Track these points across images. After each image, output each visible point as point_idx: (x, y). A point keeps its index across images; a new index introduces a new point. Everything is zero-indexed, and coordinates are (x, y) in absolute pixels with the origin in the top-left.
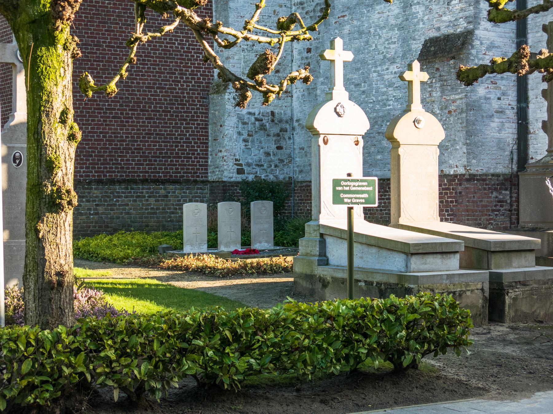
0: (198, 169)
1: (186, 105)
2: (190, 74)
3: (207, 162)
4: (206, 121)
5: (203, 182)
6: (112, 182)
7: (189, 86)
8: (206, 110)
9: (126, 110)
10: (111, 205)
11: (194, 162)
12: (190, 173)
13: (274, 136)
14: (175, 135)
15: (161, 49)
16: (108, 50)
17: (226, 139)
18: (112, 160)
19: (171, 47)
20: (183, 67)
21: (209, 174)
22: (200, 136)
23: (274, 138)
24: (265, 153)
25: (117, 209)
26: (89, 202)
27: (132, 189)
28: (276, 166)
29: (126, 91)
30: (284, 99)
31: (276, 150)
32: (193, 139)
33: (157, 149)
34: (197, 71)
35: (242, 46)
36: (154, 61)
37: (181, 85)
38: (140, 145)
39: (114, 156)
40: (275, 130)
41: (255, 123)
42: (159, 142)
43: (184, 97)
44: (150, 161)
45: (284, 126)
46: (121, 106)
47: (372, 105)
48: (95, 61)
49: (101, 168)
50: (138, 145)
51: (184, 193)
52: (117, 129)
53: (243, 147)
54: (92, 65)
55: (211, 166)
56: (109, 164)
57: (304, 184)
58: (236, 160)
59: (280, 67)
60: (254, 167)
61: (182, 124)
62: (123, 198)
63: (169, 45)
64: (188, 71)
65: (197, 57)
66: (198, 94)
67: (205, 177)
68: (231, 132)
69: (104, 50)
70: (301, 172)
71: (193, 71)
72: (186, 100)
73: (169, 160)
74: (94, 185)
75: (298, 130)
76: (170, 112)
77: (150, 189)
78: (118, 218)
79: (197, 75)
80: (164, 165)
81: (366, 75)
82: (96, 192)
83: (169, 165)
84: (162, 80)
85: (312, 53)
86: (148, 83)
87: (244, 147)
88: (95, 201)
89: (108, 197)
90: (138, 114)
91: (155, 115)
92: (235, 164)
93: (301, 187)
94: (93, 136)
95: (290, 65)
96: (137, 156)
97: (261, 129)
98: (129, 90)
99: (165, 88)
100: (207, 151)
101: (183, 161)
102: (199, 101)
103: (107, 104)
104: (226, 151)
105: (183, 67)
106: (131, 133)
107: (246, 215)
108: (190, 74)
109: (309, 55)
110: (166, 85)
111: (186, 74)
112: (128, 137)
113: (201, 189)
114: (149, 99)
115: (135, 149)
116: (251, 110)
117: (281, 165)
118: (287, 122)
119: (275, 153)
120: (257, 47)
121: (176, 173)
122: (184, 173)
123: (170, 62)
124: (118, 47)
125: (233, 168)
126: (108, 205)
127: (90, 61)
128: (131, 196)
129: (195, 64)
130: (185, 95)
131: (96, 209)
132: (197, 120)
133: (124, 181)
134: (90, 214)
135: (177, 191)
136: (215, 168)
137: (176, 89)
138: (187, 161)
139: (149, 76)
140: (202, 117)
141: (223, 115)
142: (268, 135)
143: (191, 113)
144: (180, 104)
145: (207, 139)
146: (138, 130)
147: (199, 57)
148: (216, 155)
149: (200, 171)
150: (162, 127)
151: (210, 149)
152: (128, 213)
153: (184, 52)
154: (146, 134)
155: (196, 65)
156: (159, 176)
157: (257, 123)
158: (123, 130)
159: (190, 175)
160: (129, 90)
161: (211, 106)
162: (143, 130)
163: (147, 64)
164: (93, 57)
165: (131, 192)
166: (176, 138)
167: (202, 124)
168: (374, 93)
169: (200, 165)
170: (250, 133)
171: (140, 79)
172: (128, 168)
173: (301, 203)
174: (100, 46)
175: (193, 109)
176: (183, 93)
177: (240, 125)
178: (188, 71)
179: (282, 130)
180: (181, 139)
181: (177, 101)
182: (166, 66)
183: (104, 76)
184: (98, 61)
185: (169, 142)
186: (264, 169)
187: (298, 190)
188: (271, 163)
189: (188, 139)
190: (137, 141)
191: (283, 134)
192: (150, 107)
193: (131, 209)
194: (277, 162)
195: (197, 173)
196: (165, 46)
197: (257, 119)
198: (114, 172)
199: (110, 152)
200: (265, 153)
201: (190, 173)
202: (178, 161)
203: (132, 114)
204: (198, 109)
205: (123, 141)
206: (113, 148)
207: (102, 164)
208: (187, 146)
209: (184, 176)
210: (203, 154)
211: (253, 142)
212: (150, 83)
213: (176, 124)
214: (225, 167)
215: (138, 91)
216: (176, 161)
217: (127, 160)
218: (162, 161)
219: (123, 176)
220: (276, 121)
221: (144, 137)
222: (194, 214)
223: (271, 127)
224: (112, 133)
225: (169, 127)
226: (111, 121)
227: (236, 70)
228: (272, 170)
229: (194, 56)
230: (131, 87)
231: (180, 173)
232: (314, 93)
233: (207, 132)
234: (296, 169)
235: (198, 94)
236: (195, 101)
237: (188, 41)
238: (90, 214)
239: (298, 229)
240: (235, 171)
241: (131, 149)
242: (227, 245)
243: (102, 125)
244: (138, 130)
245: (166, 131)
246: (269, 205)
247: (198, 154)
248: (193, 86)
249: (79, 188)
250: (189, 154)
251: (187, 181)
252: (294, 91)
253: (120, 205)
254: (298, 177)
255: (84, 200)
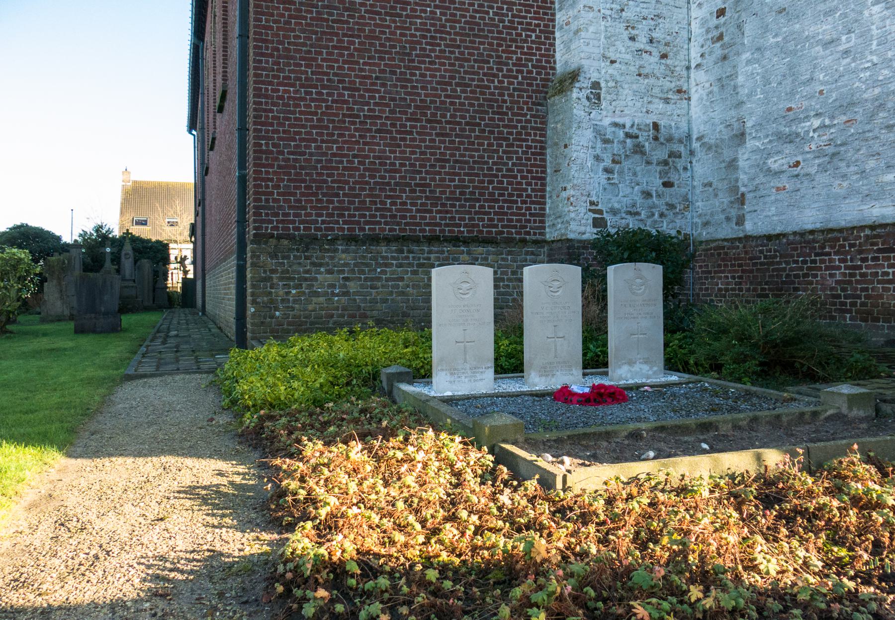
0: (529, 221)
1: (507, 114)
2: (514, 64)
3: (544, 209)
4: (542, 142)
5: (536, 242)
6: (374, 239)
7: (513, 83)
8: (541, 123)
9: (400, 119)
10: (372, 279)
11: (521, 209)
12: (515, 227)
13: (658, 164)
14: (487, 163)
15: (463, 20)
16: (370, 18)
17: (574, 167)
18: (375, 203)
19: (483, 19)
20: (503, 51)
21: (547, 230)
22: (532, 166)
23: (659, 168)
24: (643, 192)
25: (383, 286)
26: (332, 273)
27: (410, 252)
28: (662, 215)
29: (402, 87)
30: (675, 103)
31: (661, 188)
32: (518, 171)
33: (456, 187)
34: (526, 60)
35: (602, 11)
36: (451, 40)
37: (499, 82)
38: (425, 179)
39: (379, 196)
40: (661, 154)
41: (625, 142)
42: (459, 174)
43: (505, 101)
44: (444, 205)
45: (676, 147)
46: (392, 112)
47: (868, 74)
48: (345, 35)
49: (354, 216)
50: (421, 179)
51: (503, 259)
52: (385, 151)
53: (604, 182)
54: (339, 41)
55: (550, 216)
56: (370, 209)
57: (713, 245)
58: (592, 203)
59: (668, 49)
60: (624, 215)
61: (501, 146)
62: (394, 268)
63: (478, 15)
64: (511, 58)
65: (527, 36)
66: (528, 97)
67: (540, 234)
68: (582, 155)
69: (363, 17)
70: (706, 224)
71: (520, 59)
72: (507, 107)
73: (477, 204)
74: (341, 245)
75: (700, 154)
76: (479, 125)
77: (443, 252)
78: (385, 301)
79: (526, 66)
80: (470, 213)
81: (852, 15)
82: (344, 256)
83: (476, 213)
84: (466, 72)
85: (728, 14)
86: (441, 76)
87: (606, 182)
88: (343, 272)
89: (367, 265)
90: (422, 127)
91: (454, 129)
92: (590, 210)
93: (707, 250)
94: (342, 162)
95: (686, 47)
96: (420, 198)
97: (635, 152)
98: (406, 87)
99: (470, 86)
100: (544, 191)
101: (503, 207)
102: (529, 109)
103: (366, 108)
104: (574, 187)
105: (503, 51)
106: (409, 159)
107: (595, 295)
108: (514, 64)
109: (722, 20)
110: (473, 80)
111: (507, 64)
112: (405, 165)
113: (532, 253)
114: (443, 102)
115: (417, 185)
116: (617, 120)
117: (670, 214)
118: (680, 141)
119: (660, 193)
120: (629, 14)
121: (488, 226)
122: (503, 227)
123: (480, 43)
124: (387, 14)
125: (586, 217)
126: (366, 279)
127: (337, 35)
128: (409, 264)
129: (523, 48)
130: (506, 97)
131: (345, 286)
132: (527, 140)
133: (397, 239)
134: (333, 294)
135: (490, 257)
136: (556, 218)
137: (489, 88)
138: (509, 208)
139: (444, 64)
140: (535, 135)
141: (570, 127)
142: (648, 163)
143: (516, 127)
144: (498, 113)
145: (544, 172)
146: (422, 153)
147: (531, 36)
148: (558, 196)
149: (532, 224)
150: (466, 149)
151: (548, 189)
152: (403, 293)
153: (504, 27)
154: (437, 160)
155: (525, 50)
156: (459, 231)
157: (628, 141)
158: (395, 152)
159: (513, 231)
160: (406, 87)
161: (550, 116)
162: (432, 154)
163: (439, 45)
164: (343, 29)
165: (407, 258)
166: (490, 169)
167: (536, 147)
168: (874, 47)
169: (530, 214)
170: (616, 158)
171: (427, 69)
172: (405, 217)
173: (706, 278)
174: (355, 10)
175: (520, 121)
176: (502, 95)
177: (599, 145)
178: (511, 58)
179: (672, 155)
180: (497, 170)
181: (492, 107)
182: (474, 48)
183: (361, 61)
184: (350, 36)
185: (477, 175)
186: (641, 220)
187: (700, 255)
188: (654, 210)
189: (511, 170)
190: (421, 172)
191: (674, 162)
192: (444, 116)
193: (408, 286)
194: (664, 208)
195: (526, 227)
196: (471, 17)
197: (628, 135)
198: (379, 223)
199: (370, 189)
200: (643, 192)
201: (515, 227)
202: (493, 207)
203: (412, 127)
204: (527, 121)
205: (396, 171)
206: (376, 183)
207: (356, 209)
208: (509, 183)
209: (503, 232)
210: (536, 196)
211: (621, 173)
212: (444, 77)
213: (490, 145)
214: (573, 215)
215: (423, 88)
216: (490, 207)
217: (401, 204)
218: (464, 206)
219: (395, 230)
220: (662, 140)
221: (432, 166)
222: (460, 294)
223: (653, 149)
224: (374, 157)
225: (477, 150)
226: (374, 137)
227: (591, 51)
228: (655, 222)
229: (521, 35)
230: (411, 81)
231: (496, 226)
232: (732, 83)
233: (544, 160)
234: (696, 220)
235: (528, 97)
236: (522, 109)
237: (512, 10)
238: (333, 294)
239: (725, 331)
240: (590, 221)
241: (409, 185)
242: (546, 371)
243: (358, 143)
244: (422, 153)
245: (472, 157)
246: (651, 275)
247: (528, 196)
248: (519, 83)
249: (314, 249)
250: (513, 195)
251: (509, 241)
252: (693, 90)
253: (387, 280)
254: (700, 234)
255: (322, 269)
